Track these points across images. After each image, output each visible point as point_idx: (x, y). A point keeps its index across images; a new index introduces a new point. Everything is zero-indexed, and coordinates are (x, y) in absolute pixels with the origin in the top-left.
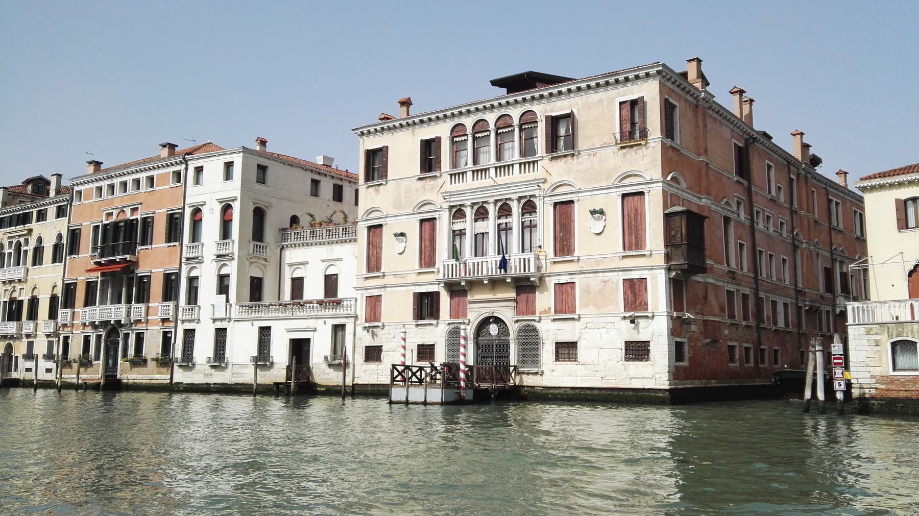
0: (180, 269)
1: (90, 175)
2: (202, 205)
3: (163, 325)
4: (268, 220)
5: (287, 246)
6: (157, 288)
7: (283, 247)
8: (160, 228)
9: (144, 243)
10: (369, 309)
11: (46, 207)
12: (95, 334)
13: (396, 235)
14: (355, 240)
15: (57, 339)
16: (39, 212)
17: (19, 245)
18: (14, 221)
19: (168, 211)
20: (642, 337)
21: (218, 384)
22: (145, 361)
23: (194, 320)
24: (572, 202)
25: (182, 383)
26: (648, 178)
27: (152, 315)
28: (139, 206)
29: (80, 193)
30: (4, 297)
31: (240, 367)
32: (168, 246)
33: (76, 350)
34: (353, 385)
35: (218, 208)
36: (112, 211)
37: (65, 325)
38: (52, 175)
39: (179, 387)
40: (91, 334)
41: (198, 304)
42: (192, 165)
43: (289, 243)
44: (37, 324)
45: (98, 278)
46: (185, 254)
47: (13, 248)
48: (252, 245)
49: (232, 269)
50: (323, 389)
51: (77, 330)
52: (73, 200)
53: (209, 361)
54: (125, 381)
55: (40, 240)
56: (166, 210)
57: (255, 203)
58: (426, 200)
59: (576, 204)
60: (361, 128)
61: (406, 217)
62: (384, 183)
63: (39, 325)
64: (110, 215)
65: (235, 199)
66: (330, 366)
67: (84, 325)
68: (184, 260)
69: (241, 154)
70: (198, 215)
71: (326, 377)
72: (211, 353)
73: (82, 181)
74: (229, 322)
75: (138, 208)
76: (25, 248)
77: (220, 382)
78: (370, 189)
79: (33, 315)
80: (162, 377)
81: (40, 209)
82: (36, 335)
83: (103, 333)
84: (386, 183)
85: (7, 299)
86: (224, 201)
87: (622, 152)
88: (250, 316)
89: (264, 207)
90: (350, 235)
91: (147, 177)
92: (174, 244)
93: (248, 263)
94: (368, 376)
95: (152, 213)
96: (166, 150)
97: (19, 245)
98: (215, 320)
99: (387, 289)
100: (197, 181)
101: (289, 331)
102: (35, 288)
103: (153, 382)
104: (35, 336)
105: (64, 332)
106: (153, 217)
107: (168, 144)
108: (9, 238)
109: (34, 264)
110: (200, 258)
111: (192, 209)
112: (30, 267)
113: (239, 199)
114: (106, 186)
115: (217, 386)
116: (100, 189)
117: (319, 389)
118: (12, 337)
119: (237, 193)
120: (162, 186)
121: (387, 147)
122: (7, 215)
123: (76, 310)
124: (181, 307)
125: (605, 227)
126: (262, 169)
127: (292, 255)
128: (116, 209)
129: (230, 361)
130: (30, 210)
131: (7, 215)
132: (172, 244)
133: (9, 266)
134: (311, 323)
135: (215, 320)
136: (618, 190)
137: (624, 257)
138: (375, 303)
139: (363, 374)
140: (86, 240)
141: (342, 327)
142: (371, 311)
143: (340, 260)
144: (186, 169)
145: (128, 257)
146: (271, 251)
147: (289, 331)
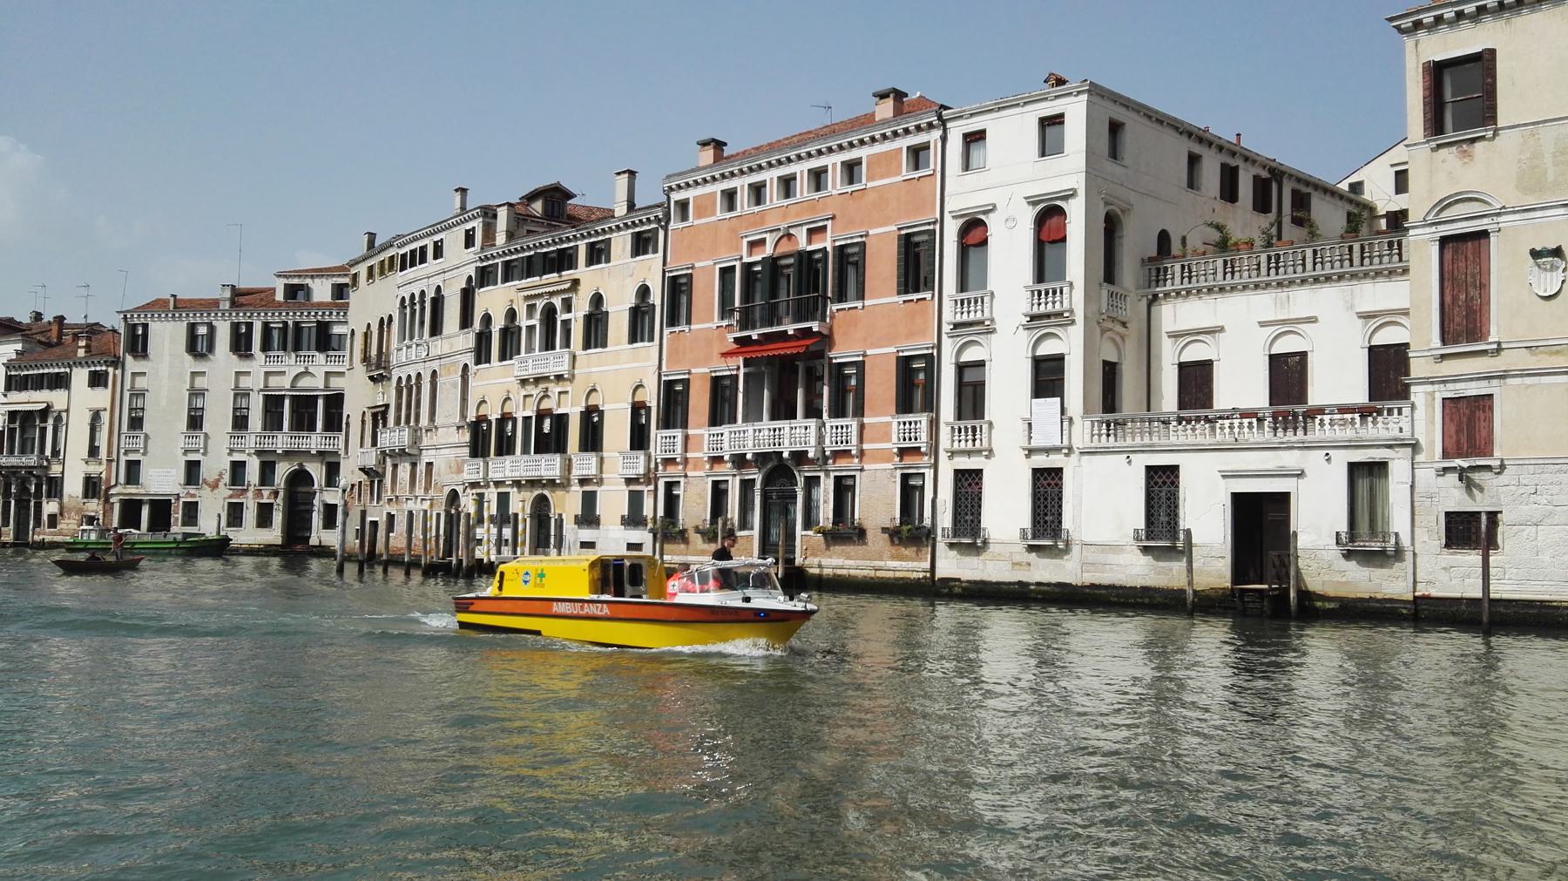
0: (939, 346)
1: (704, 168)
2: (986, 212)
3: (901, 460)
4: (1125, 240)
5: (1167, 295)
6: (881, 385)
8: (883, 265)
9: (841, 296)
10: (1453, 429)
11: (607, 236)
12: (738, 478)
13: (1535, 254)
14: (1405, 271)
15: (652, 487)
16: (591, 246)
17: (550, 312)
18: (538, 265)
19: (899, 229)
20: (1480, 504)
21: (1048, 585)
22: (683, 532)
23: (979, 452)
24: (1484, 234)
25: (959, 580)
27: (872, 441)
28: (829, 223)
29: (683, 206)
30: (524, 410)
31: (1103, 551)
32: (904, 302)
33: (694, 508)
34: (1415, 597)
35: (1028, 215)
36: (825, 223)
37: (669, 462)
38: (619, 174)
39: (951, 588)
40: (730, 478)
41: (987, 418)
42: (956, 132)
43: (1169, 287)
44: (602, 458)
45: (738, 368)
46: (949, 316)
47: (538, 315)
48: (1105, 293)
49: (1070, 344)
50: (1329, 606)
51: (695, 469)
52: (670, 219)
53: (1137, 539)
54: (816, 571)
55: (597, 300)
56: (895, 228)
57: (1107, 204)
58: (1461, 193)
59: (1493, 238)
60: (1418, 12)
62: (1490, 134)
63: (605, 460)
64: (753, 245)
65: (1069, 195)
66: (1348, 555)
67: (716, 460)
68: (946, 328)
69: (1085, 97)
70: (1053, 222)
71: (1338, 578)
73: (690, 181)
74: (1067, 455)
75: (825, 227)
76: (566, 316)
77: (1054, 581)
79: (592, 439)
80: (910, 566)
81: (592, 240)
82: (602, 479)
83: (757, 476)
84: (1495, 135)
85: (530, 412)
86: (1041, 201)
88: (1120, 443)
89: (1119, 213)
90: (1290, 269)
92: (920, 296)
93: (1098, 329)
95: (861, 236)
96: (889, 104)
97: (550, 312)
99: (1509, 381)
102: (594, 390)
103: (880, 574)
104: (600, 482)
105: (665, 475)
106: (864, 244)
107: (714, 140)
108: (527, 298)
109: (587, 345)
110: (987, 323)
111: (961, 221)
112: (580, 352)
114: (746, 187)
115: (1046, 588)
116: (730, 196)
117: (1319, 604)
118: (552, 483)
119: (1078, 182)
120: (882, 177)
121: (1492, 52)
122: (521, 255)
123: (690, 432)
124: (947, 424)
125: (1563, 282)
126: (1115, 128)
127: (1175, 315)
128: (771, 231)
129: (1074, 536)
130: (571, 244)
131: (521, 255)
132: (915, 296)
133: (530, 349)
134: (1290, 459)
135: (1031, 452)
136: (1433, 229)
137: (1443, 357)
138: (1473, 413)
140: (706, 293)
143: (1312, 320)
144: (944, 139)
145: (815, 326)
146: (1134, 309)
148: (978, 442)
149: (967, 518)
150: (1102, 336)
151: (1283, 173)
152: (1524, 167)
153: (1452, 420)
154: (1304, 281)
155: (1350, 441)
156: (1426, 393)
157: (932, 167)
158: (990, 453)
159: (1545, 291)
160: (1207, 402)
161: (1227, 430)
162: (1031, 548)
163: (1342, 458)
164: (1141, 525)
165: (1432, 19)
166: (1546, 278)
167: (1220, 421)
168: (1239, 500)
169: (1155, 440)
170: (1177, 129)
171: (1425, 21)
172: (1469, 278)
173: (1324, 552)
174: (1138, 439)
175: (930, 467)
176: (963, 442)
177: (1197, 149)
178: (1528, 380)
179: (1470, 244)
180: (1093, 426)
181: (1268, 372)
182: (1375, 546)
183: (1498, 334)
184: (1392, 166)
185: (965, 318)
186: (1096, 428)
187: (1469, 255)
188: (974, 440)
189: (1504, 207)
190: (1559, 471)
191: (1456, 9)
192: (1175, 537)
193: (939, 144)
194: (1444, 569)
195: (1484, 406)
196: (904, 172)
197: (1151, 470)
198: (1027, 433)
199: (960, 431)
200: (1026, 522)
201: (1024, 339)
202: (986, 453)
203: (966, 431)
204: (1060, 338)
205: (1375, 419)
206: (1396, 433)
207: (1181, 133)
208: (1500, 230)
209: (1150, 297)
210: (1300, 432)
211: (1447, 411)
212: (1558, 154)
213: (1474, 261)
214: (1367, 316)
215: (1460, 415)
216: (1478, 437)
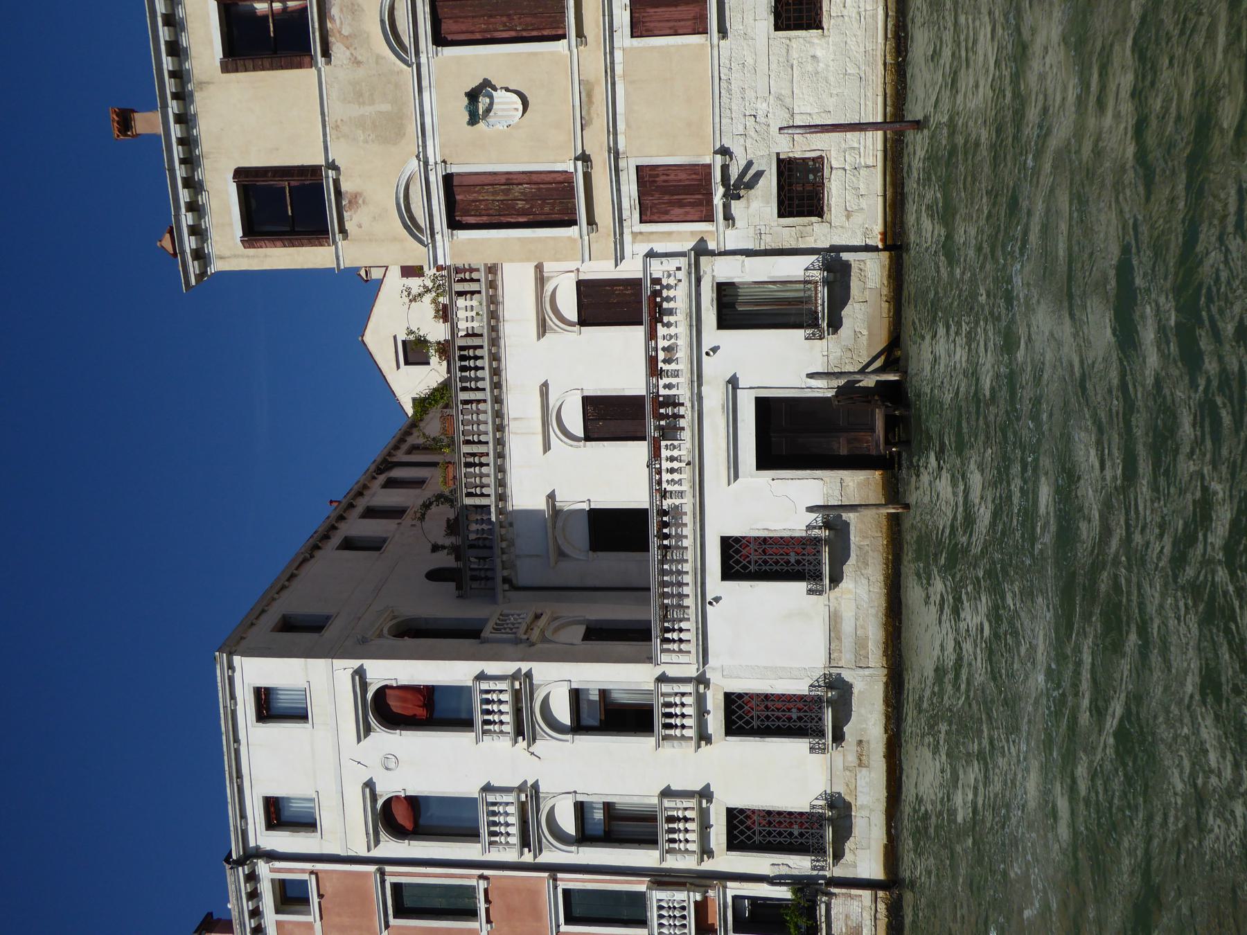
2: (374, 797)
7: (506, 580)
10: (677, 211)
24: (448, 179)
26: (414, 165)
31: (839, 639)
34: (886, 248)
35: (385, 740)
57: (380, 636)
58: (382, 21)
59: (454, 169)
61: (426, 95)
62: (331, 173)
65: (360, 673)
66: (835, 324)
68: (528, 857)
69: (237, 660)
70: (395, 705)
72: (795, 748)
74: (707, 683)
78: (348, 226)
84: (335, 167)
87: (337, 50)
88: (691, 613)
91: (278, 912)
93: (539, 646)
94: (863, 203)
98: (704, 737)
99: (621, 147)
100: (307, 824)
101: (734, 472)
110: (523, 798)
111: (383, 835)
113: (355, 663)
119: (344, 668)
124: (662, 859)
125: (507, 90)
132: (482, 906)
134: (714, 397)
136: (438, 237)
137: (591, 222)
139: (858, 219)
141: (725, 292)
142: (681, 204)
144: (272, 856)
147: (734, 472)
148: (689, 814)
149: (796, 827)
150: (550, 641)
151: (385, 461)
152: (373, 136)
153: (666, 213)
154: (498, 400)
155: (691, 326)
156: (633, 242)
157: (305, 877)
158: (705, 794)
159: (517, 109)
160: (639, 516)
161: (676, 476)
162: (838, 737)
163: (711, 334)
164: (801, 586)
165: (193, 238)
166: (503, 110)
167: (664, 485)
168: (766, 460)
169: (687, 567)
170: (305, 561)
171: (194, 246)
172: (498, 198)
173: (831, 357)
174: (686, 590)
175: (725, 887)
176: (689, 836)
177: (336, 540)
178: (621, 126)
179: (458, 197)
180: (668, 651)
181: (605, 443)
182: (823, 293)
183: (564, 162)
184: (398, 367)
185: (513, 830)
186: (670, 646)
187: (471, 198)
188: (686, 820)
189: (418, 156)
190: (729, 91)
191: (183, 210)
192: (816, 541)
193: (278, 865)
194: (848, 217)
195: (650, 176)
196: (309, 919)
197: (729, 573)
198: (676, 743)
199: (673, 841)
200: (800, 746)
201: (550, 746)
202: (704, 802)
203: (669, 715)
204: (548, 695)
205: (664, 299)
206: (681, 275)
207: (312, 556)
208: (444, 162)
209: (506, 587)
210: (682, 411)
211: (655, 218)
212: (361, 100)
213: (479, 192)
214: (543, 328)
215: (660, 204)
216: (687, 183)
